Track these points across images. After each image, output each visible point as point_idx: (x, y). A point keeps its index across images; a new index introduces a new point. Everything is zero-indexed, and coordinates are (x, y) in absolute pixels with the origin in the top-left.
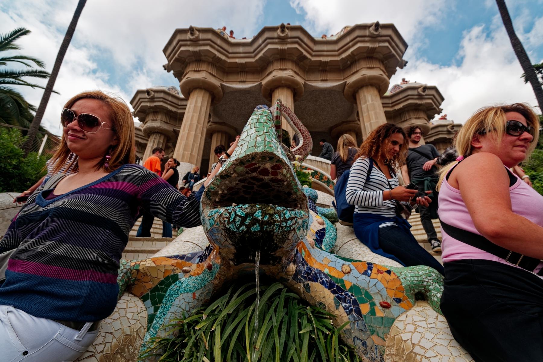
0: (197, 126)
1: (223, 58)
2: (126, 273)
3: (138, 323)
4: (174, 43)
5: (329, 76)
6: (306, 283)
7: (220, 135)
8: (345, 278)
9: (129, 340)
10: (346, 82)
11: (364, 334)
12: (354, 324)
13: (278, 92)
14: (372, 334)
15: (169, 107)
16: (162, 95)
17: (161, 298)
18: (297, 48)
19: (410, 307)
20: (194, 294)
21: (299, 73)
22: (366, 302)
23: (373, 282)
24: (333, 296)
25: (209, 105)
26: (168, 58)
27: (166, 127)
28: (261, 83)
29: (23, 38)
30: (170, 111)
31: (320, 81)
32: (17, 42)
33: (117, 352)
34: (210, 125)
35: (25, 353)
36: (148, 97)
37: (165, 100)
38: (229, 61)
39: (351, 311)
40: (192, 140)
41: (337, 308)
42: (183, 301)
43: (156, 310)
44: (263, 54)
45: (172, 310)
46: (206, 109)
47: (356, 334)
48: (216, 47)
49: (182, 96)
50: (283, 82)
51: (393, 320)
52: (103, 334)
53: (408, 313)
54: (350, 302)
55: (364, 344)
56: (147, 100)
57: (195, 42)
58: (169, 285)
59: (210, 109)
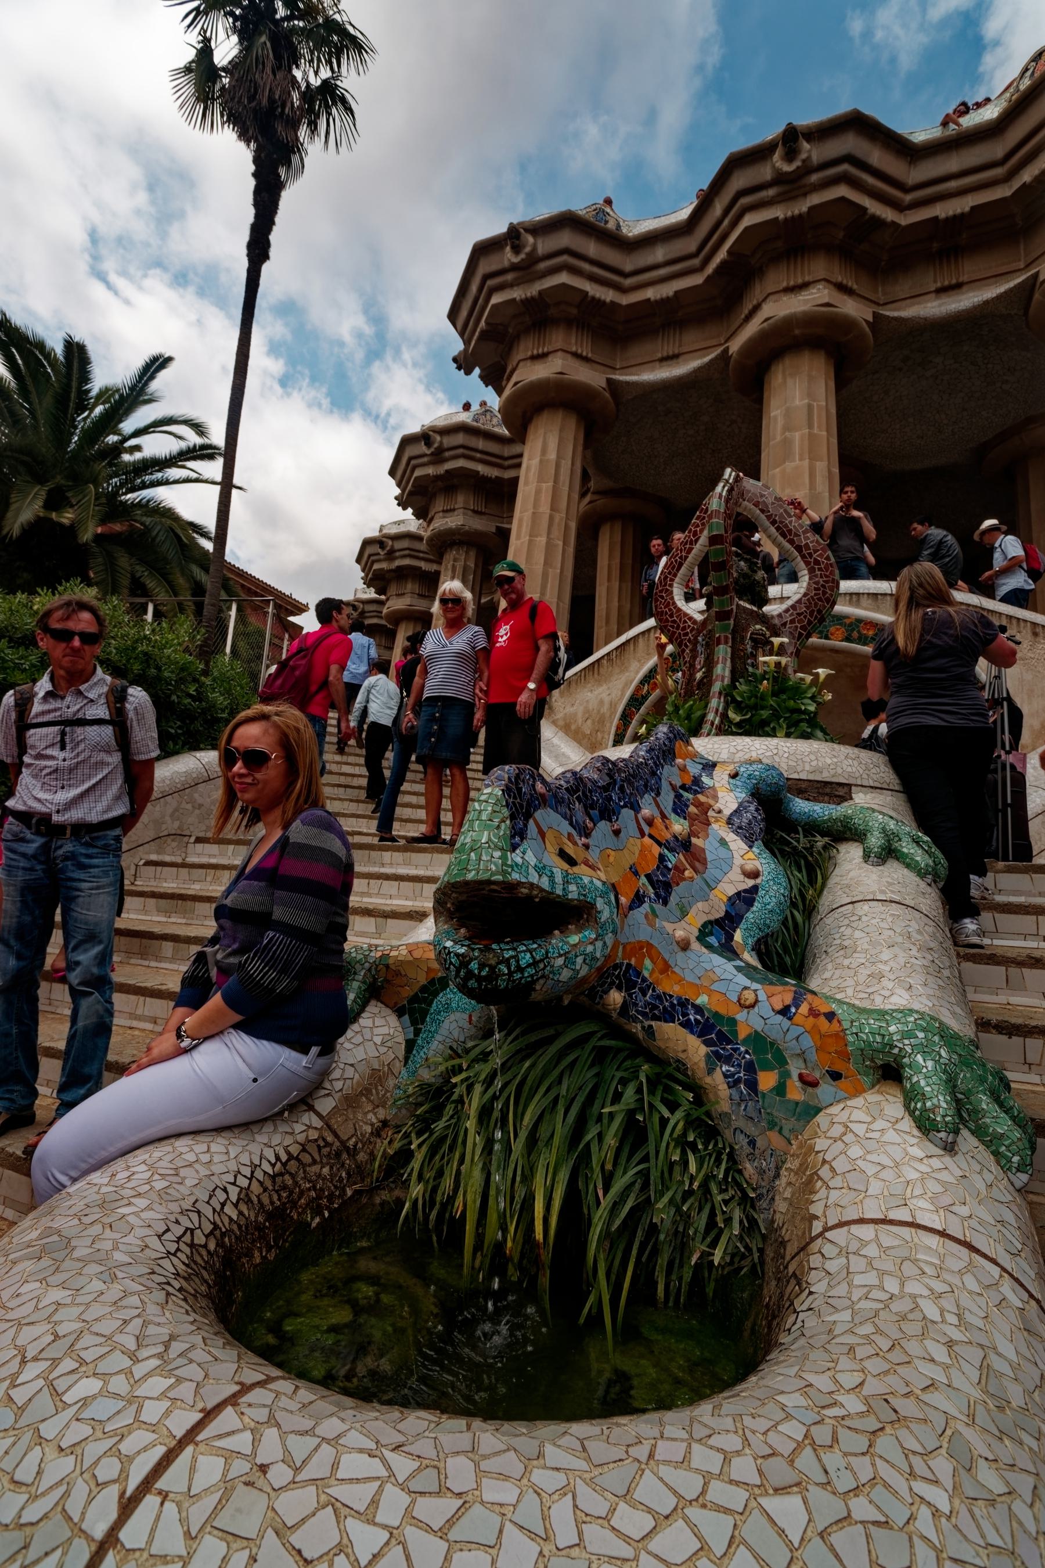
0: (551, 519)
1: (608, 295)
2: (369, 970)
3: (390, 1052)
4: (474, 288)
5: (969, 269)
6: (647, 1023)
7: (618, 527)
8: (741, 1016)
9: (377, 1077)
10: (1036, 276)
11: (755, 1125)
12: (739, 1105)
13: (781, 367)
14: (770, 1129)
15: (481, 468)
16: (460, 439)
17: (425, 1013)
18: (843, 199)
19: (858, 1092)
20: (470, 1016)
21: (855, 287)
22: (772, 1069)
23: (795, 1031)
24: (703, 1050)
25: (580, 448)
26: (462, 334)
27: (478, 524)
28: (727, 350)
29: (163, 376)
30: (486, 479)
31: (933, 295)
32: (155, 386)
33: (361, 1094)
34: (590, 502)
35: (255, 1080)
36: (428, 452)
37: (468, 451)
38: (625, 300)
39: (737, 1082)
40: (542, 561)
41: (710, 1071)
42: (455, 1024)
43: (417, 1032)
44: (730, 252)
45: (439, 1038)
46: (573, 464)
47: (741, 1123)
48: (586, 267)
49: (504, 431)
50: (797, 332)
51: (818, 1110)
52: (342, 1066)
53: (849, 1103)
54: (739, 1065)
55: (752, 1143)
56: (425, 459)
57: (527, 270)
58: (436, 994)
59: (584, 457)
